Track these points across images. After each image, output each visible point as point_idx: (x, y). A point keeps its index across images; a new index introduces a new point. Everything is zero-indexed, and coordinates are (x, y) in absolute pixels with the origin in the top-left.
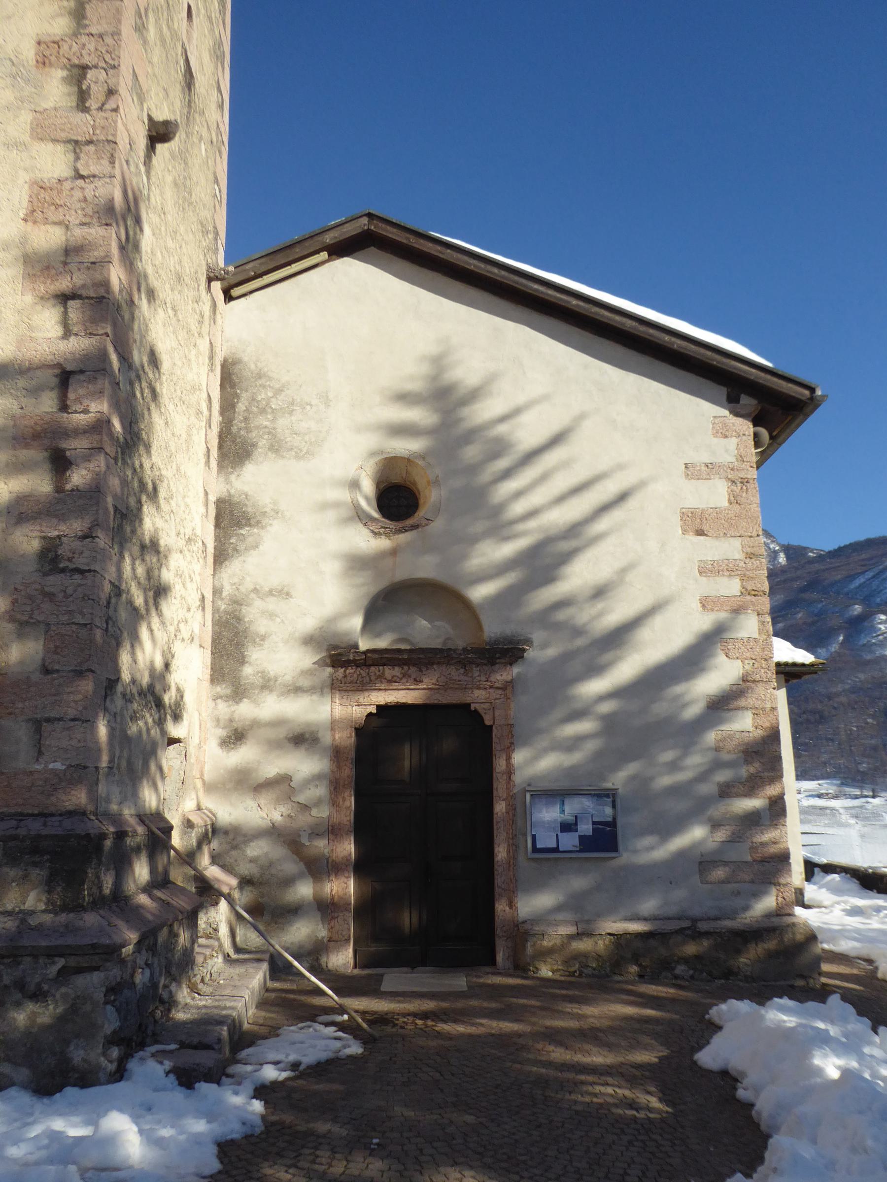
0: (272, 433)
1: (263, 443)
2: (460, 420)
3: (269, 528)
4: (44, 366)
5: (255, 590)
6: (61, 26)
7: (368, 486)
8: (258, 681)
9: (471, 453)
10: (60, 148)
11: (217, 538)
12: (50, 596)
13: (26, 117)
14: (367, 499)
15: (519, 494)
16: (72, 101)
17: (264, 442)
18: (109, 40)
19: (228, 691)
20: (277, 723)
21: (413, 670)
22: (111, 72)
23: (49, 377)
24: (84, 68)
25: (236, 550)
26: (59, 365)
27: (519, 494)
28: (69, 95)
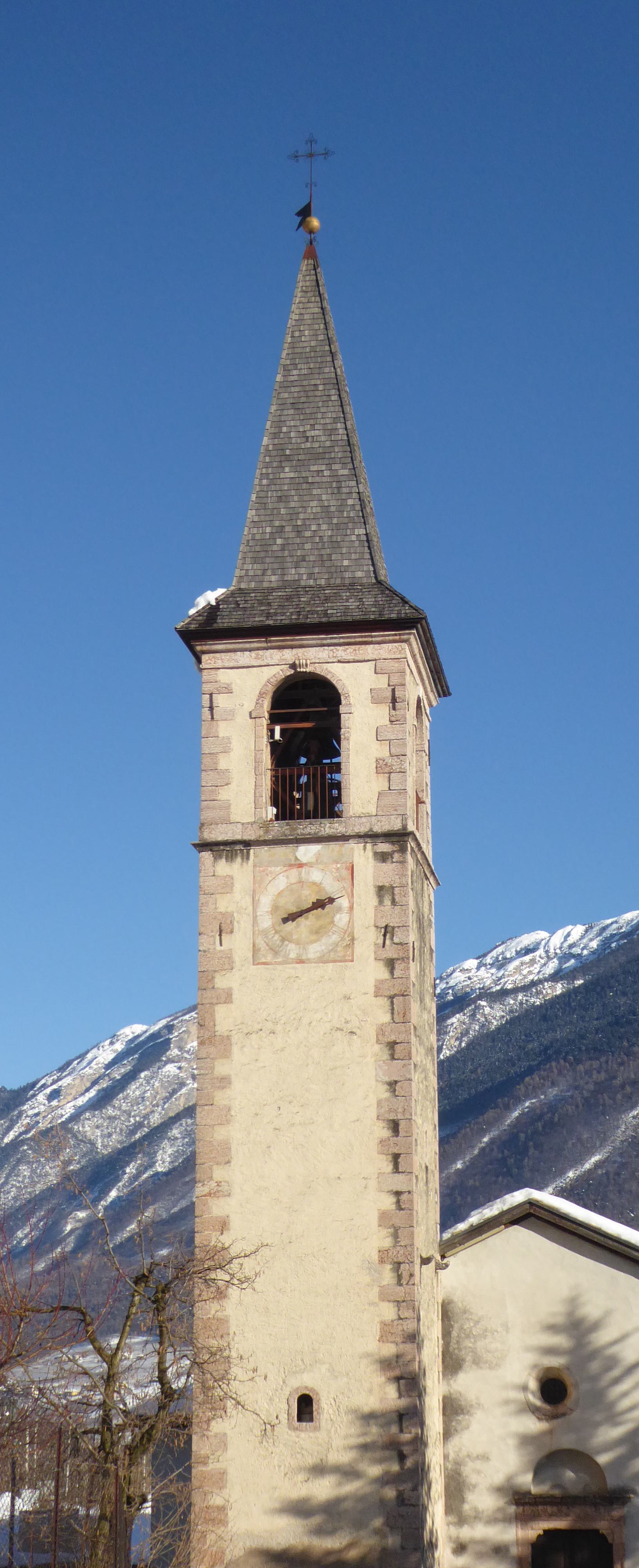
0: (474, 1351)
1: (469, 1358)
2: (589, 1343)
3: (475, 1416)
4: (391, 1412)
5: (468, 1456)
6: (388, 1243)
7: (533, 1385)
8: (473, 1514)
9: (595, 1366)
10: (391, 1305)
11: (444, 1422)
12: (402, 1516)
13: (376, 1290)
14: (533, 1393)
15: (625, 1394)
16: (395, 1281)
17: (470, 1358)
18: (409, 1249)
19: (456, 1520)
20: (482, 1542)
21: (564, 1509)
22: (411, 1265)
23: (395, 1416)
24: (399, 1263)
25: (456, 1430)
26: (398, 1411)
27: (625, 1394)
28: (394, 1277)
